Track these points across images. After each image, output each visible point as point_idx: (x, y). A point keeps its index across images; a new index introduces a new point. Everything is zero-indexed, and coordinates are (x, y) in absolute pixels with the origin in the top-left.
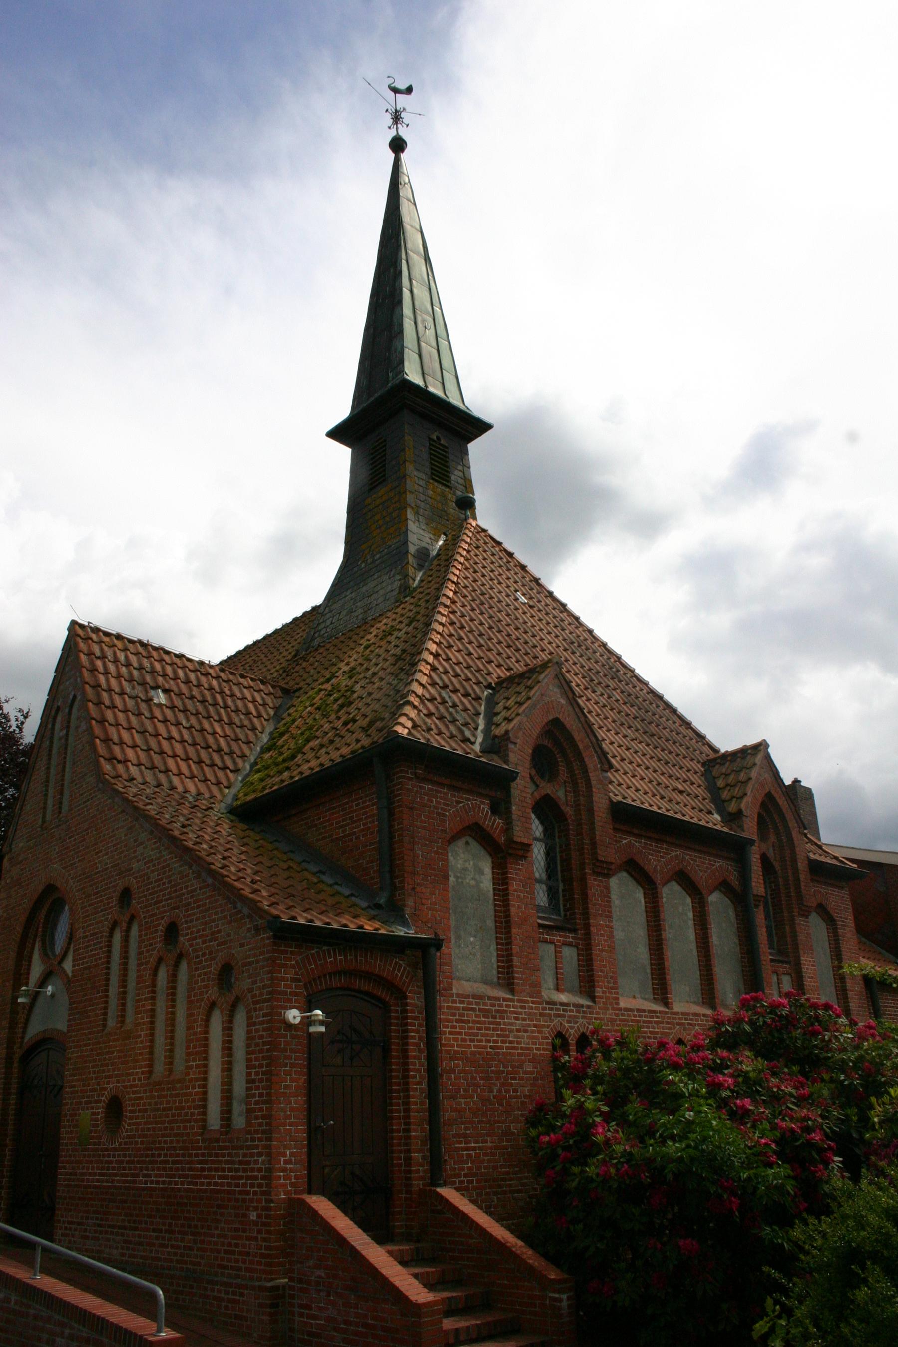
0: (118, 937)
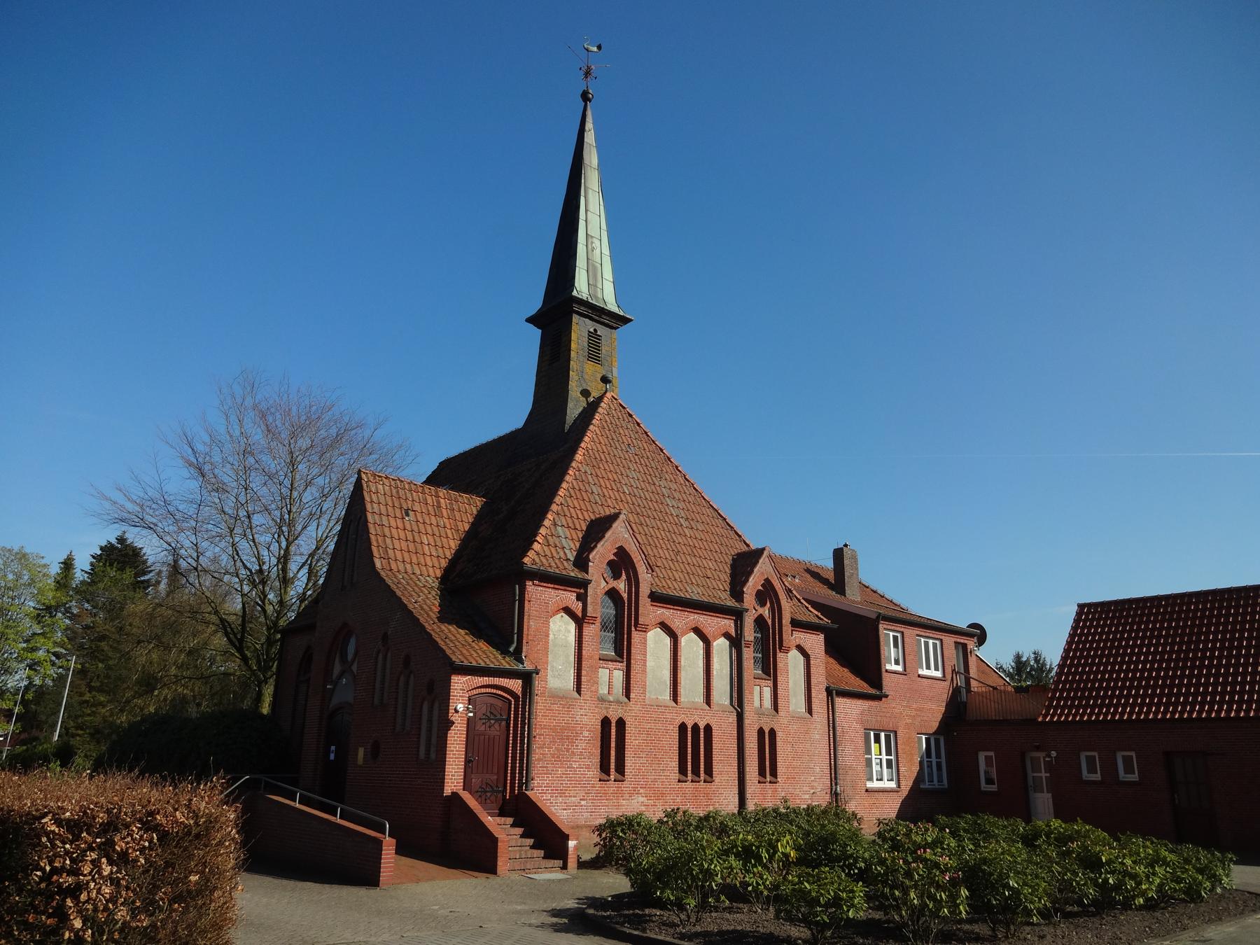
0: (381, 656)
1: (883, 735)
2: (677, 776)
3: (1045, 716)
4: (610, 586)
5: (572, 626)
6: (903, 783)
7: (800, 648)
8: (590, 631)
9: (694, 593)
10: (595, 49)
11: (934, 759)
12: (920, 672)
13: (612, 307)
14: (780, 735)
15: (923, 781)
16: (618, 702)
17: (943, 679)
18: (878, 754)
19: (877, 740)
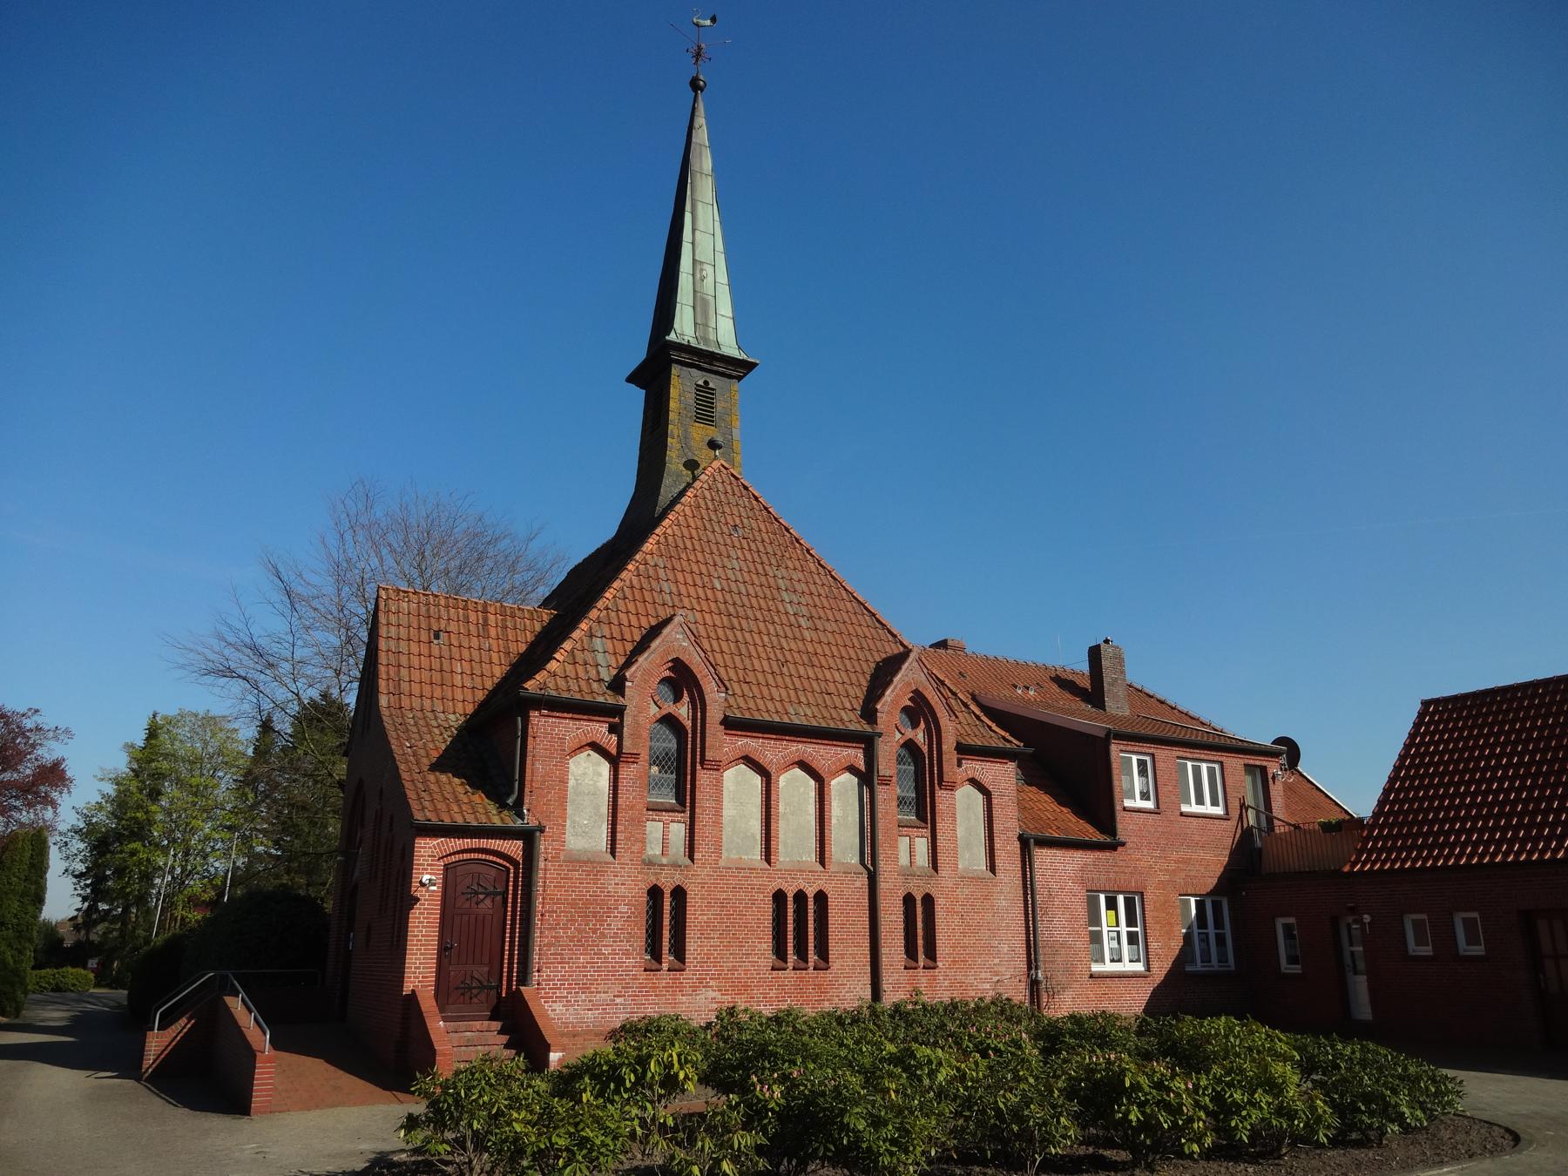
1: (1121, 899)
2: (771, 958)
3: (1354, 864)
4: (664, 712)
5: (605, 768)
6: (1155, 965)
7: (974, 782)
8: (627, 772)
9: (799, 715)
10: (708, 22)
11: (1211, 930)
12: (1185, 808)
13: (730, 348)
14: (940, 904)
15: (1193, 961)
16: (675, 866)
17: (1226, 817)
18: (1113, 925)
19: (1111, 904)
